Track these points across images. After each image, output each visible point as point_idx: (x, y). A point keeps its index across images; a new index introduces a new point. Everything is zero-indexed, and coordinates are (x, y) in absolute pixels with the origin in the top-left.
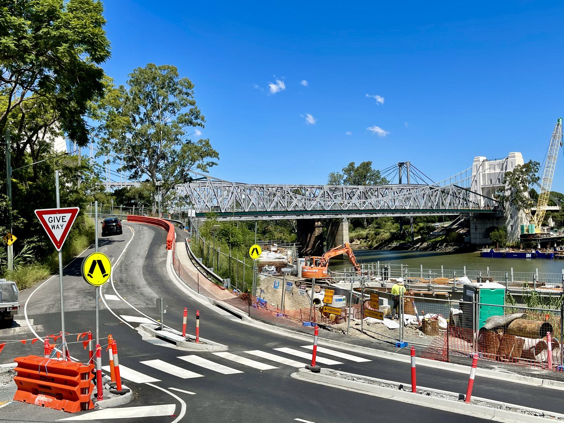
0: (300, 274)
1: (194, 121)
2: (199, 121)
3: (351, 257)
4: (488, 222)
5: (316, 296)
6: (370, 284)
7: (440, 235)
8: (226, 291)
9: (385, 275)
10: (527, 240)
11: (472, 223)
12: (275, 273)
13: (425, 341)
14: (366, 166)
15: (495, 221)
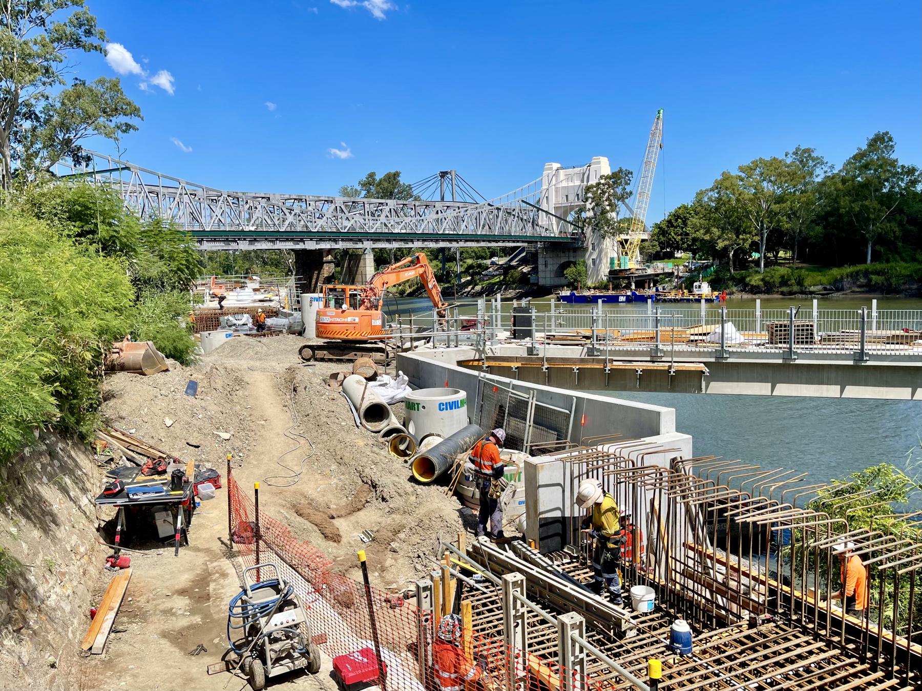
0: (311, 331)
1: (83, 39)
2: (93, 40)
3: (430, 286)
4: (562, 254)
10: (617, 277)
11: (540, 256)
12: (251, 329)
14: (393, 178)
15: (572, 254)
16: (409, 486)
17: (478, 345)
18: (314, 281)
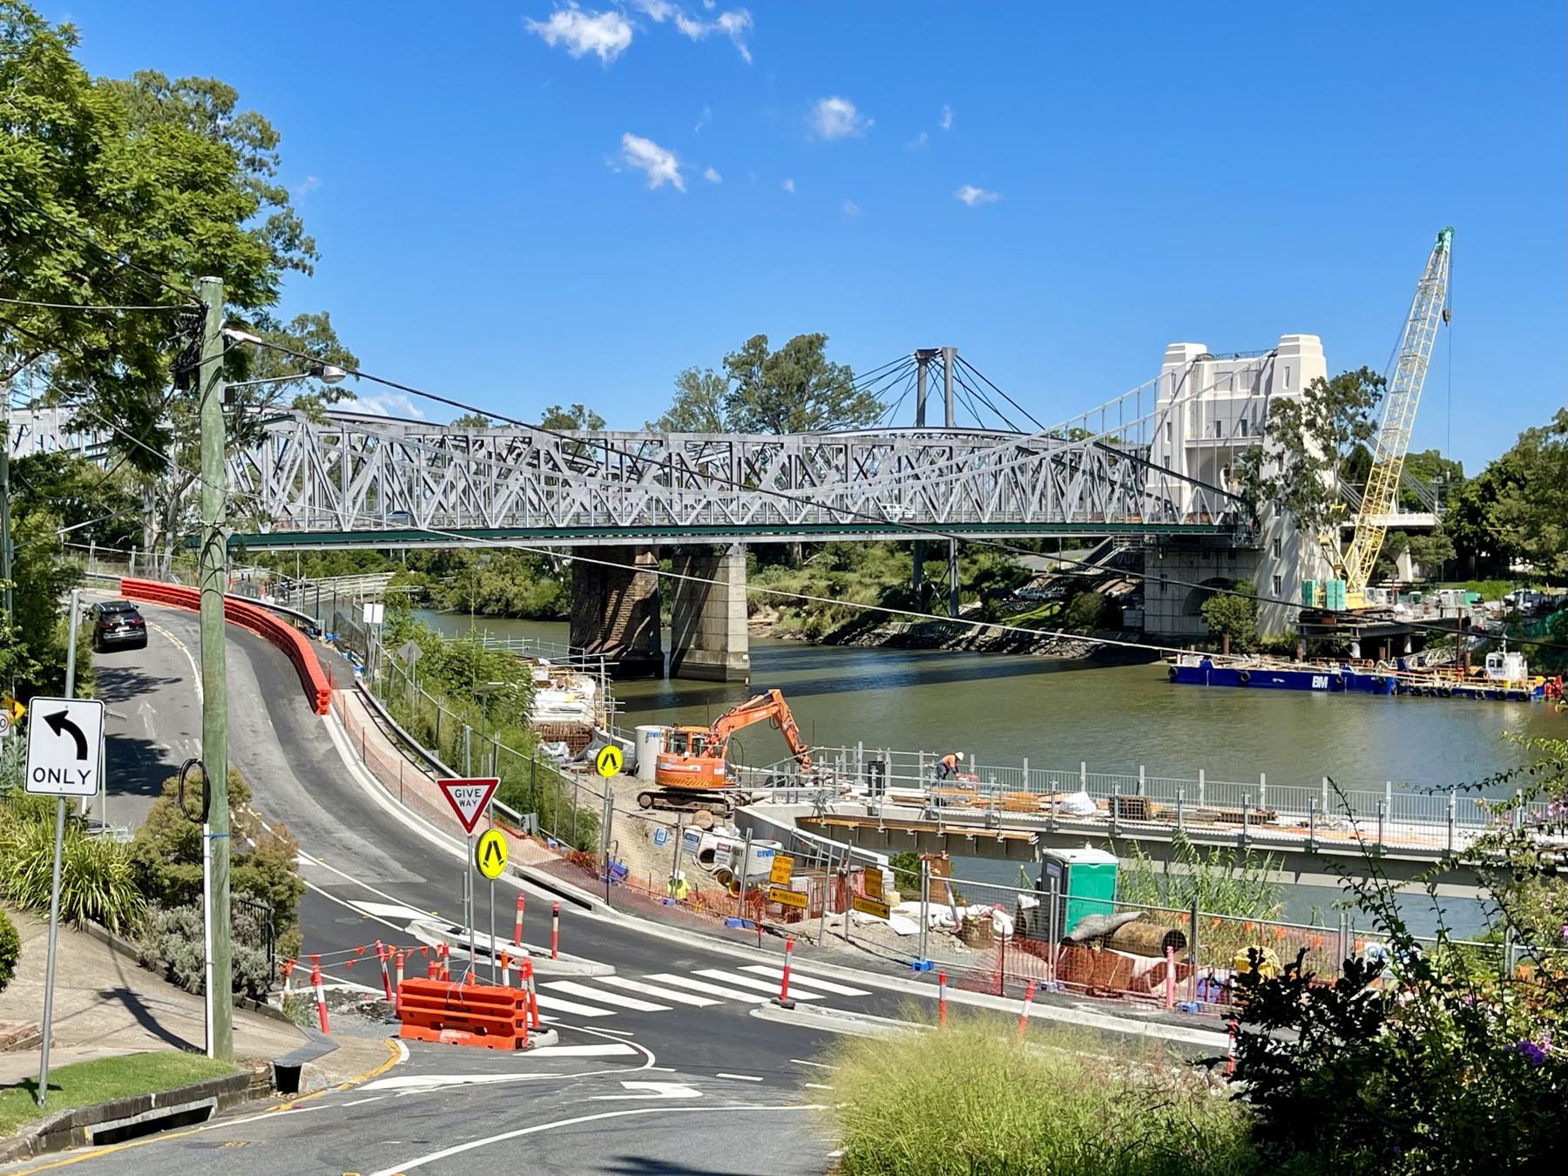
2: (296, 255)
4: (1203, 562)
5: (709, 842)
6: (840, 807)
7: (1047, 601)
8: (529, 842)
9: (879, 786)
10: (1321, 632)
11: (1149, 563)
13: (965, 957)
14: (807, 350)
15: (1225, 561)
16: (726, 900)
17: (818, 800)
18: (610, 609)
